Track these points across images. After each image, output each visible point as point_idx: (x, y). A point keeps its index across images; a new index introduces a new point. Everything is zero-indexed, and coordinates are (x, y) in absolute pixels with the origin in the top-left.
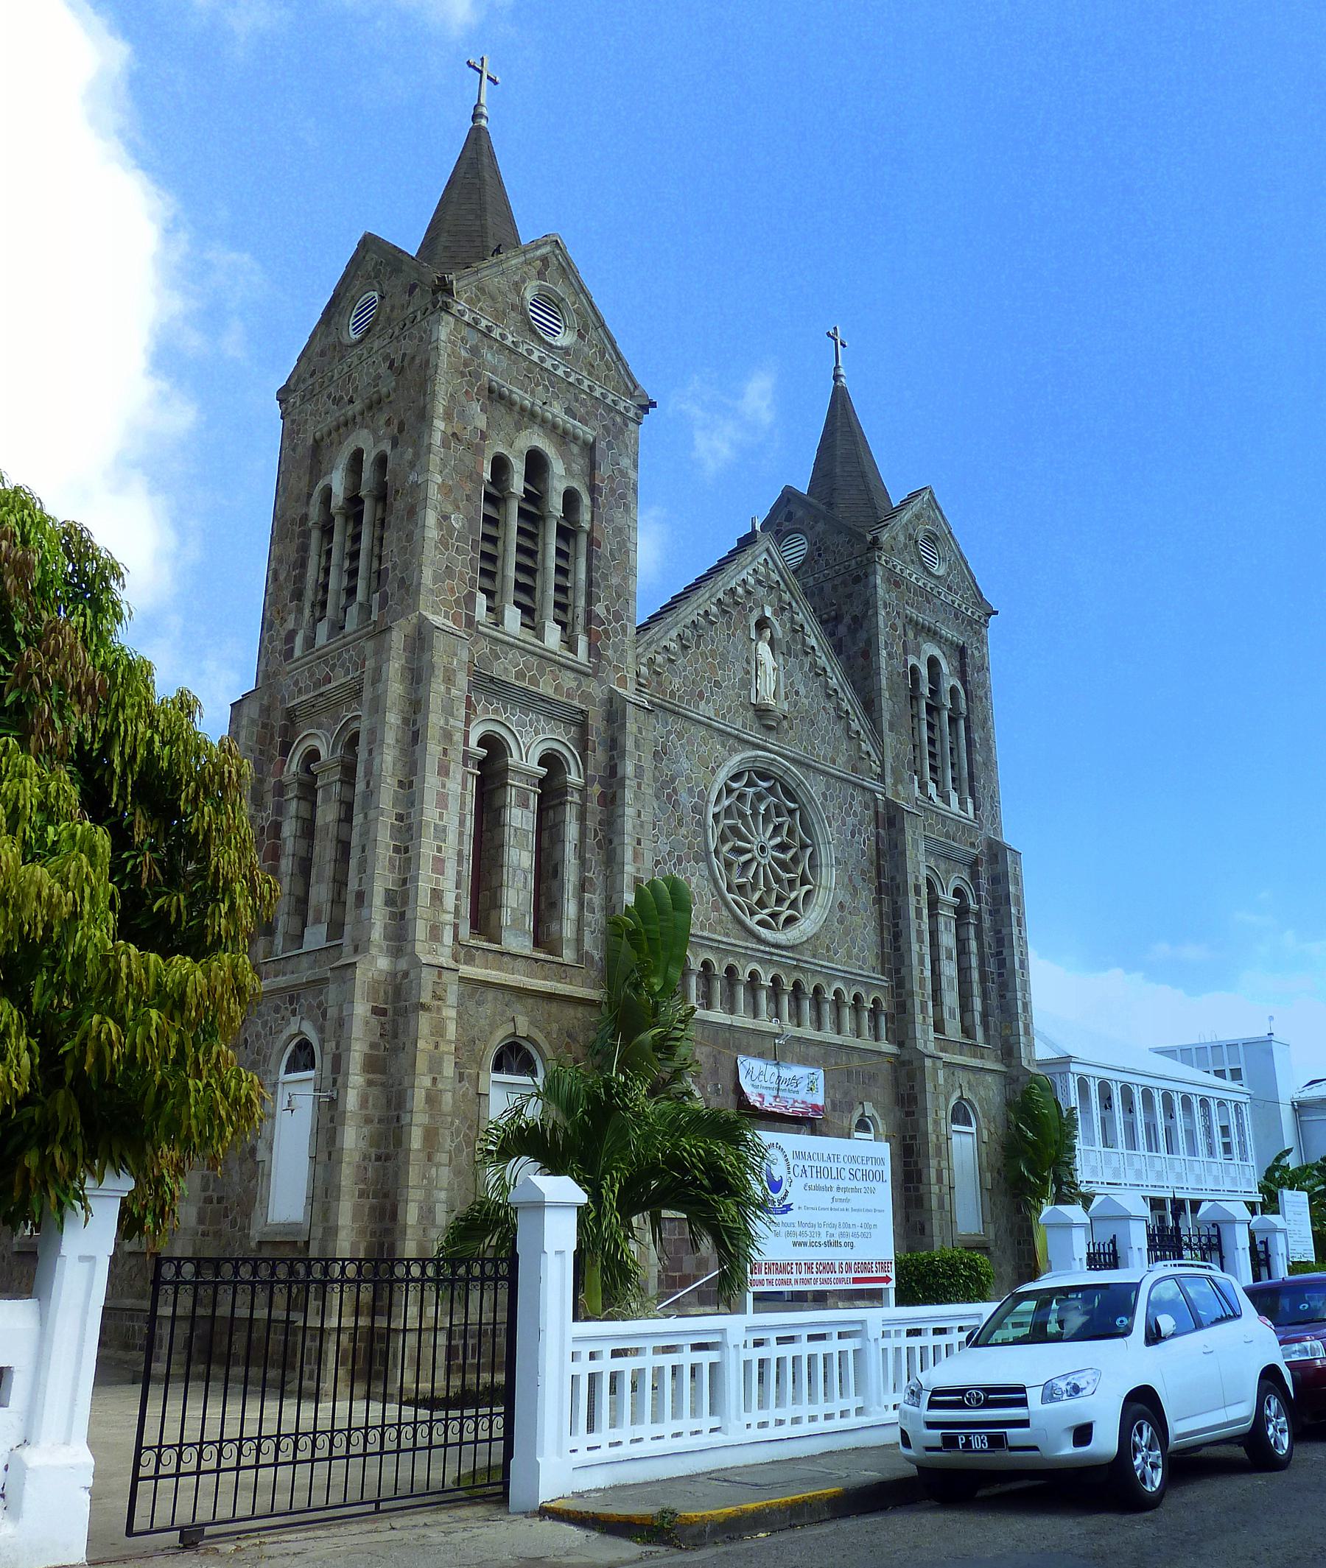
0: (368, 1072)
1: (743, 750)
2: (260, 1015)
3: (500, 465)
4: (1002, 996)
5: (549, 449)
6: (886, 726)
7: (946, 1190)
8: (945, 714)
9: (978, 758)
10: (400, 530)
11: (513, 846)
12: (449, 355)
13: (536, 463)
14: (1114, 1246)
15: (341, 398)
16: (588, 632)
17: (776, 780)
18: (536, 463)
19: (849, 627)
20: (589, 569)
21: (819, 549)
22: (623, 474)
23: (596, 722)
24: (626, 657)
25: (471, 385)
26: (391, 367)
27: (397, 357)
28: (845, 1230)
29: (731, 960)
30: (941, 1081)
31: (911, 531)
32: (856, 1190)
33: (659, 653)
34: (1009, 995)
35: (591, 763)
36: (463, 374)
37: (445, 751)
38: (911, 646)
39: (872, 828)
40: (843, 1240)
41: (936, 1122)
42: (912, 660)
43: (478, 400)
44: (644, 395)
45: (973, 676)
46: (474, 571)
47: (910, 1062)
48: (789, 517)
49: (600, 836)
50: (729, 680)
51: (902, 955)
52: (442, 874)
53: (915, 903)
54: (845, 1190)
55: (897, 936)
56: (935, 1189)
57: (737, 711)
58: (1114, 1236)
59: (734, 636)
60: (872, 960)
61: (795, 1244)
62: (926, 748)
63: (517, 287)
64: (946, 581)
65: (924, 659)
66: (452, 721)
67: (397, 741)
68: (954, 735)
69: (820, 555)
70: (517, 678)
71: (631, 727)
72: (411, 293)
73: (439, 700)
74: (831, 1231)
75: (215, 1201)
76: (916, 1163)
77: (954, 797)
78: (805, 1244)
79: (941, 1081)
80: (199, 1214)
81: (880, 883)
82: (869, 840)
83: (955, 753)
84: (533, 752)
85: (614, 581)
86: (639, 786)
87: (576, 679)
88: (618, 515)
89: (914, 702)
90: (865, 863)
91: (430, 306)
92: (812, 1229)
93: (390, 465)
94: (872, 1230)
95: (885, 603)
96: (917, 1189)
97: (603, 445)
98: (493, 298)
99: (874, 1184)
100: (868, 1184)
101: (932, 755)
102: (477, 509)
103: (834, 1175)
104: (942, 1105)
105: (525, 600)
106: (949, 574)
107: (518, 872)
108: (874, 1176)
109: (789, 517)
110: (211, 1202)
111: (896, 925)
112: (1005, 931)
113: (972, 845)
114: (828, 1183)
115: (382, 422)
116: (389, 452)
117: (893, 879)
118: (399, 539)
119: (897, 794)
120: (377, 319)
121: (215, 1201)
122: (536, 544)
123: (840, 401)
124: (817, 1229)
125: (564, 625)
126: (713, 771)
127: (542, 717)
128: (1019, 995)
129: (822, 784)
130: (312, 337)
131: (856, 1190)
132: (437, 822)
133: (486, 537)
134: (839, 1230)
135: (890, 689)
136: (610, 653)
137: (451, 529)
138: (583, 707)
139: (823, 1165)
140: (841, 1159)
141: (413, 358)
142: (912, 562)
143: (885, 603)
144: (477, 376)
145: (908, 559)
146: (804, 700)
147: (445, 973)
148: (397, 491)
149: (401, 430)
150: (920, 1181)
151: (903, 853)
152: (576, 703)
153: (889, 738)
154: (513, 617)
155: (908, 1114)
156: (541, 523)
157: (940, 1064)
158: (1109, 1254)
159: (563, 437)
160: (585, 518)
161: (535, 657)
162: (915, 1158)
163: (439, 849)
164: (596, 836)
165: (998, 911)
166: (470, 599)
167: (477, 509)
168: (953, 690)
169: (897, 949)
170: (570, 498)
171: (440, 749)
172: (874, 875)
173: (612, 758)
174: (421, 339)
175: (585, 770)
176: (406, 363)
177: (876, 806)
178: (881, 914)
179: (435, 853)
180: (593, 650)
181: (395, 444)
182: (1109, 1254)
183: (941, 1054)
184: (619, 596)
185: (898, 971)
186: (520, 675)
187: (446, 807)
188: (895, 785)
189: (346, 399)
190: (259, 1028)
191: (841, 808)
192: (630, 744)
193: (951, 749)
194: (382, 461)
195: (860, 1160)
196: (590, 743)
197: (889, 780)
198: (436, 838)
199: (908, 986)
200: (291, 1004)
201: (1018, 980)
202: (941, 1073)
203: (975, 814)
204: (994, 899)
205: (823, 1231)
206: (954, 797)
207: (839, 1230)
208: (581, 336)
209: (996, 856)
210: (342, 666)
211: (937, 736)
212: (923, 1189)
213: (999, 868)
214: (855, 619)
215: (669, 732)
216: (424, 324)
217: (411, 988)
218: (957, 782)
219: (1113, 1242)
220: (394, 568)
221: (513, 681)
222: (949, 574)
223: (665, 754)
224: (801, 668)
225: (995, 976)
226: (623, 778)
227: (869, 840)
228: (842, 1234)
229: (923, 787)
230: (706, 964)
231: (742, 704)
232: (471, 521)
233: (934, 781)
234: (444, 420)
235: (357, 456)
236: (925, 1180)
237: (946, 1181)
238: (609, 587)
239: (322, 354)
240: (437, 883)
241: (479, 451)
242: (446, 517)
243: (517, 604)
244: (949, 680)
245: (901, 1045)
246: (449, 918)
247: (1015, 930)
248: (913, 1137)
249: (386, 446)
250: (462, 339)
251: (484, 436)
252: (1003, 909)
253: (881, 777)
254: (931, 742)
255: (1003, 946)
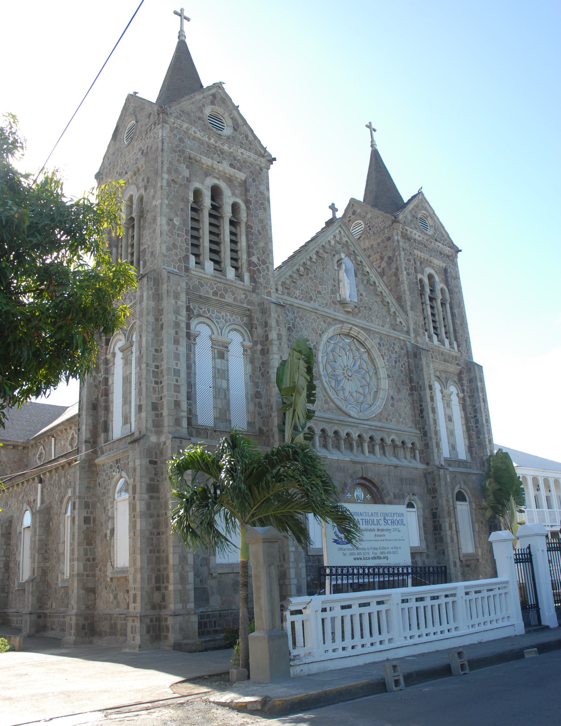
0: (150, 492)
1: (335, 324)
2: (104, 471)
3: (197, 194)
4: (478, 437)
5: (223, 185)
6: (409, 308)
7: (454, 532)
8: (439, 301)
9: (458, 322)
10: (150, 228)
11: (217, 378)
12: (168, 143)
13: (216, 192)
14: (530, 550)
15: (122, 172)
16: (249, 271)
17: (354, 338)
18: (216, 192)
19: (387, 262)
20: (248, 240)
21: (369, 226)
22: (262, 193)
23: (257, 315)
24: (270, 282)
25: (180, 156)
26: (142, 154)
27: (145, 148)
28: (383, 551)
29: (336, 428)
30: (449, 480)
31: (414, 213)
32: (388, 530)
33: (287, 279)
34: (481, 436)
35: (255, 335)
36: (175, 152)
37: (177, 333)
38: (419, 269)
39: (405, 359)
40: (382, 556)
41: (448, 501)
42: (419, 276)
43: (184, 163)
44: (270, 155)
45: (452, 282)
46: (187, 244)
47: (433, 472)
48: (354, 213)
49: (262, 370)
50: (325, 290)
51: (425, 420)
52: (179, 393)
53: (429, 393)
54: (382, 530)
55: (422, 411)
56: (449, 533)
57: (330, 305)
58: (529, 545)
59: (326, 268)
60: (410, 424)
61: (355, 559)
62: (430, 318)
63: (201, 109)
64: (434, 236)
65: (426, 275)
66: (179, 317)
67: (153, 330)
68: (445, 312)
69: (370, 229)
70: (213, 295)
71: (274, 315)
72: (149, 118)
73: (172, 307)
74: (375, 551)
75: (91, 560)
76: (438, 521)
77: (447, 342)
78: (361, 559)
79: (449, 480)
80: (84, 566)
81: (411, 386)
82: (404, 364)
83: (446, 320)
84: (225, 331)
85: (261, 244)
86: (280, 344)
87: (244, 294)
88: (260, 213)
89: (423, 297)
90: (403, 377)
91: (157, 121)
92: (364, 551)
93: (144, 199)
94: (398, 550)
95: (403, 249)
96: (440, 534)
97: (250, 180)
98: (189, 115)
99: (398, 526)
100: (395, 527)
101: (434, 322)
102: (187, 215)
103: (375, 523)
104: (450, 492)
105: (215, 257)
106: (435, 234)
107: (221, 390)
108: (398, 522)
109: (354, 213)
110: (89, 561)
111: (421, 406)
112: (477, 405)
113: (458, 364)
114: (372, 527)
115: (140, 180)
116: (144, 193)
117: (418, 383)
118: (150, 233)
119: (417, 342)
120: (135, 133)
121: (91, 560)
122: (220, 230)
123: (375, 157)
124: (367, 551)
125: (236, 268)
126: (320, 335)
127: (228, 314)
128: (486, 436)
129: (378, 339)
130: (109, 147)
131: (388, 530)
132: (175, 367)
133: (192, 228)
134: (379, 551)
135: (409, 290)
136: (261, 280)
137: (174, 225)
138: (249, 307)
139: (369, 518)
140: (379, 515)
141: (151, 147)
142: (416, 228)
143: (403, 249)
144: (183, 151)
145: (413, 226)
146: (366, 299)
147: (184, 441)
148: (148, 211)
149: (148, 182)
150: (441, 529)
151: (422, 370)
152: (245, 305)
153: (411, 314)
154: (209, 266)
155: (433, 498)
156: (222, 220)
157: (447, 472)
158: (527, 554)
159: (230, 180)
160: (243, 215)
161: (222, 284)
162: (438, 519)
163: (177, 381)
164: (260, 370)
165: (473, 396)
166: (186, 258)
167: (187, 215)
168: (442, 290)
169: (422, 417)
170: (235, 207)
171: (174, 331)
172: (408, 382)
173: (266, 331)
174: (154, 138)
175: (252, 339)
176: (148, 150)
177: (407, 348)
178: (413, 401)
179: (175, 383)
180: (253, 279)
181: (146, 189)
182: (527, 554)
183: (448, 467)
184: (264, 252)
185: (424, 428)
186: (215, 294)
187: (179, 360)
188: (416, 337)
189: (124, 172)
190: (104, 477)
191: (388, 350)
192: (273, 323)
193: (444, 319)
194: (141, 199)
195: (389, 515)
196: (254, 325)
197: (412, 335)
198: (175, 375)
199: (429, 435)
200: (117, 464)
201: (485, 429)
202: (448, 476)
203: (458, 349)
204: (471, 390)
205: (371, 551)
206: (447, 342)
207: (379, 551)
208: (235, 130)
209: (470, 369)
210: (129, 298)
211: (436, 312)
212: (443, 533)
213: (472, 375)
214: (389, 258)
215: (295, 318)
216: (155, 130)
217: (167, 450)
218: (448, 334)
219: (529, 548)
220: (148, 248)
221: (211, 296)
222: (435, 234)
223: (294, 328)
224: (362, 282)
225: (474, 428)
226: (272, 340)
227: (404, 364)
228: (382, 553)
229: (430, 337)
230: (323, 431)
231: (333, 302)
232: (184, 222)
233: (436, 334)
234: (167, 173)
235: (131, 199)
236: (443, 529)
237: (454, 528)
238: (258, 248)
239: (113, 154)
240: (177, 397)
241: (187, 187)
242: (171, 220)
243: (211, 260)
244: (440, 285)
245: (428, 464)
246: (185, 414)
247: (482, 404)
248: (436, 509)
249: (142, 191)
250: (174, 135)
251: (189, 180)
252: (475, 395)
253: (408, 333)
254: (433, 315)
255: (477, 413)
